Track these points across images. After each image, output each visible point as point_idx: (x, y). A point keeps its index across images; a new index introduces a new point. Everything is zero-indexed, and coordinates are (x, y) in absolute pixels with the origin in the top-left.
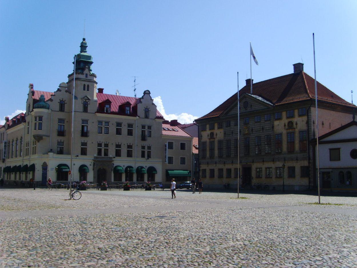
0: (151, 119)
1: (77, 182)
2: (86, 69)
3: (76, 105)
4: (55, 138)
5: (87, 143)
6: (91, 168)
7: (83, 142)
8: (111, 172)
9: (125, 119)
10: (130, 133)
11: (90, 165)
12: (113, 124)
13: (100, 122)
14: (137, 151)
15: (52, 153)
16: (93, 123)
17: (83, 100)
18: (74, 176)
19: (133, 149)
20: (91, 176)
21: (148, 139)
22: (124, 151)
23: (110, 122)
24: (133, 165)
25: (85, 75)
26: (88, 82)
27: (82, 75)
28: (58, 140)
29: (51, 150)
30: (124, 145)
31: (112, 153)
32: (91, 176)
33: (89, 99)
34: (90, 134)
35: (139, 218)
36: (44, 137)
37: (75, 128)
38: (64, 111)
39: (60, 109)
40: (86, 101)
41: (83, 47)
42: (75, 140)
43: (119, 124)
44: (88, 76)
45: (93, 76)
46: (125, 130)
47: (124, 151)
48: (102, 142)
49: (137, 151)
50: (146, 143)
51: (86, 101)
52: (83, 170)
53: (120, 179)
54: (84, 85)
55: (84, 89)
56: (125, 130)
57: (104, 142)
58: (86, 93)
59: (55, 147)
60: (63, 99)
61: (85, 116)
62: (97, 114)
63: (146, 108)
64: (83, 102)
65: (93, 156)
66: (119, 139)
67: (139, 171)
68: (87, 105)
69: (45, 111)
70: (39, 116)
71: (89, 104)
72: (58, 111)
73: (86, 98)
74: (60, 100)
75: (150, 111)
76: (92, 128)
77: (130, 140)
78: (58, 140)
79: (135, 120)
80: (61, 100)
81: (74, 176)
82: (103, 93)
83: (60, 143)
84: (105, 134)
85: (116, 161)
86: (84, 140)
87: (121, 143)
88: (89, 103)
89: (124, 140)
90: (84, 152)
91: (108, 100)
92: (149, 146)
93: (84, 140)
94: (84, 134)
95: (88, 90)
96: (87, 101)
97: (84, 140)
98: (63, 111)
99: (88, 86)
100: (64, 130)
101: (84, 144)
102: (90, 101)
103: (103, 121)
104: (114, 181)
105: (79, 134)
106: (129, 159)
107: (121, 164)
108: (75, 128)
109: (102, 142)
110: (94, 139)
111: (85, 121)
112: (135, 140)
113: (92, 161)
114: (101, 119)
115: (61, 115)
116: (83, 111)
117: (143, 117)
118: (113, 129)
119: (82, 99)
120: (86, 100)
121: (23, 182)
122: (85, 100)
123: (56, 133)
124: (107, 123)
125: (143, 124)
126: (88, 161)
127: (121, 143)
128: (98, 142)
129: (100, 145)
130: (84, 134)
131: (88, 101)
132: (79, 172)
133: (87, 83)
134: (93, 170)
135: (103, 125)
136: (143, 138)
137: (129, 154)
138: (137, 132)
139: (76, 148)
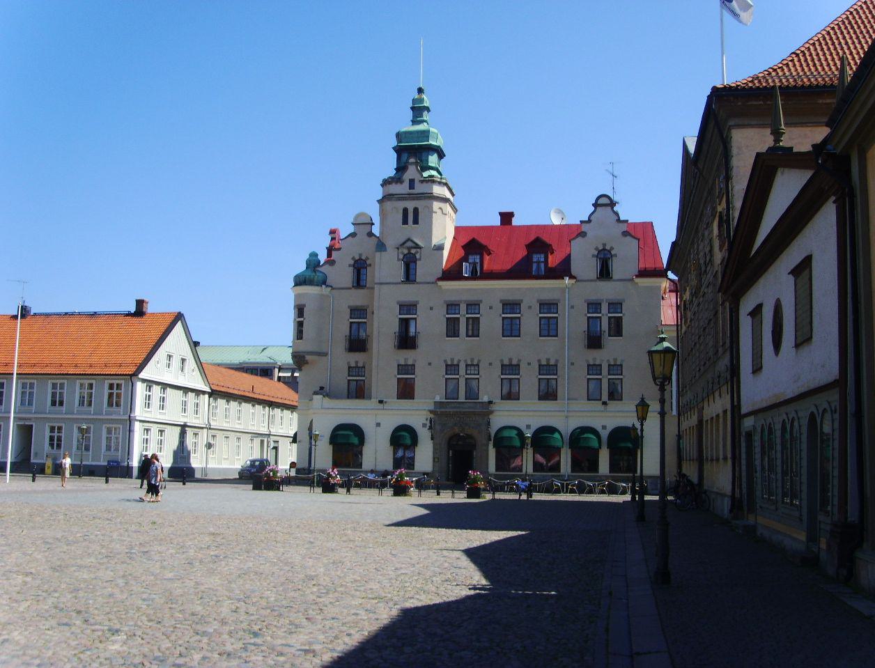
0: (621, 280)
1: (385, 474)
2: (410, 167)
3: (387, 267)
4: (342, 358)
5: (414, 365)
6: (424, 435)
7: (402, 363)
8: (487, 445)
9: (530, 290)
10: (549, 328)
11: (424, 425)
12: (491, 308)
13: (452, 306)
14: (572, 379)
15: (320, 397)
16: (431, 309)
17: (400, 250)
18: (377, 454)
19: (395, 376)
20: (424, 457)
21: (610, 343)
22: (529, 381)
23: (481, 301)
24: (596, 423)
25: (406, 184)
26: (405, 202)
27: (399, 184)
28: (587, 361)
29: (322, 388)
30: (529, 364)
31: (489, 389)
32: (424, 457)
33: (417, 247)
34: (421, 342)
35: (251, 585)
36: (308, 358)
37: (383, 326)
38: (415, 281)
39: (353, 282)
40: (409, 253)
41: (418, 111)
42: (384, 360)
43: (511, 306)
44: (417, 184)
45: (430, 184)
46: (530, 321)
47: (529, 381)
48: (459, 361)
49: (572, 379)
50: (602, 357)
51: (409, 253)
52: (403, 438)
53: (594, 466)
54: (405, 211)
55: (405, 222)
56: (530, 321)
57: (466, 361)
58: (411, 231)
59: (342, 379)
60: (360, 255)
61: (409, 293)
62: (440, 283)
63: (601, 248)
64: (401, 257)
65: (432, 401)
66: (512, 349)
67: (581, 441)
68: (415, 262)
69: (310, 292)
70: (465, 301)
71: (420, 259)
72: (350, 288)
73: (409, 244)
74: (353, 258)
75: (596, 249)
76: (429, 323)
77: (548, 349)
78: (348, 363)
79: (563, 290)
80: (357, 258)
81: (377, 454)
82: (513, 224)
83: (354, 370)
84: (468, 336)
85: (501, 413)
86: (406, 360)
87: (519, 361)
88: (418, 256)
89: (529, 349)
90: (406, 391)
91: (537, 240)
92: (451, 365)
93: (407, 356)
94: (406, 341)
95: (416, 221)
96: (413, 251)
97: (405, 359)
98: (414, 281)
99: (416, 211)
100: (601, 330)
101: (406, 368)
102: (422, 250)
103: (461, 301)
104: (497, 470)
105: (582, 341)
106: (405, 403)
107: (521, 423)
108: (383, 326)
109: (459, 361)
110: (436, 349)
111: (408, 308)
112: (566, 347)
113: (429, 413)
114: (453, 298)
115: (357, 298)
116: (598, 278)
117: (592, 278)
118: (491, 321)
119: (398, 248)
120: (409, 249)
121: (257, 463)
122: (406, 251)
123: (341, 345)
124: (473, 306)
125: (593, 298)
126: (416, 414)
127: (519, 361)
128: (445, 361)
129: (451, 368)
130: (406, 341)
131: (417, 252)
132: (391, 444)
133: (410, 205)
134: (432, 439)
135: (602, 312)
136: (594, 342)
137: (548, 394)
138: (573, 322)
139: (383, 378)
